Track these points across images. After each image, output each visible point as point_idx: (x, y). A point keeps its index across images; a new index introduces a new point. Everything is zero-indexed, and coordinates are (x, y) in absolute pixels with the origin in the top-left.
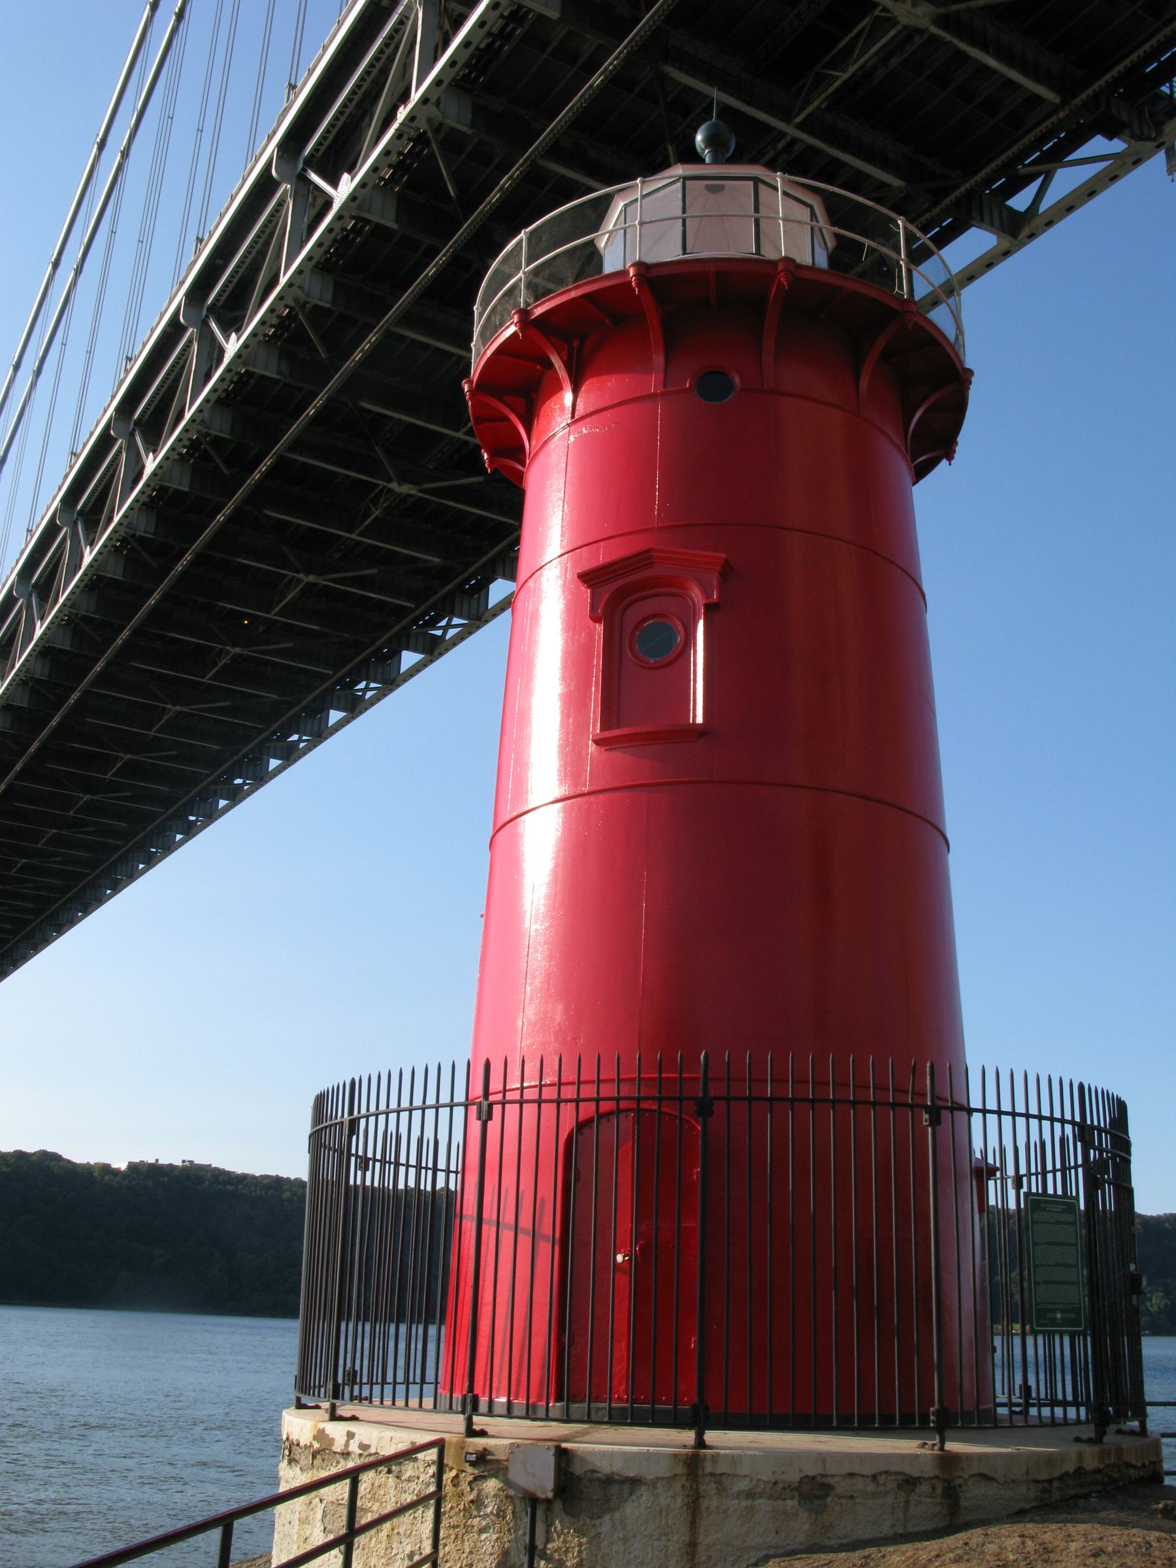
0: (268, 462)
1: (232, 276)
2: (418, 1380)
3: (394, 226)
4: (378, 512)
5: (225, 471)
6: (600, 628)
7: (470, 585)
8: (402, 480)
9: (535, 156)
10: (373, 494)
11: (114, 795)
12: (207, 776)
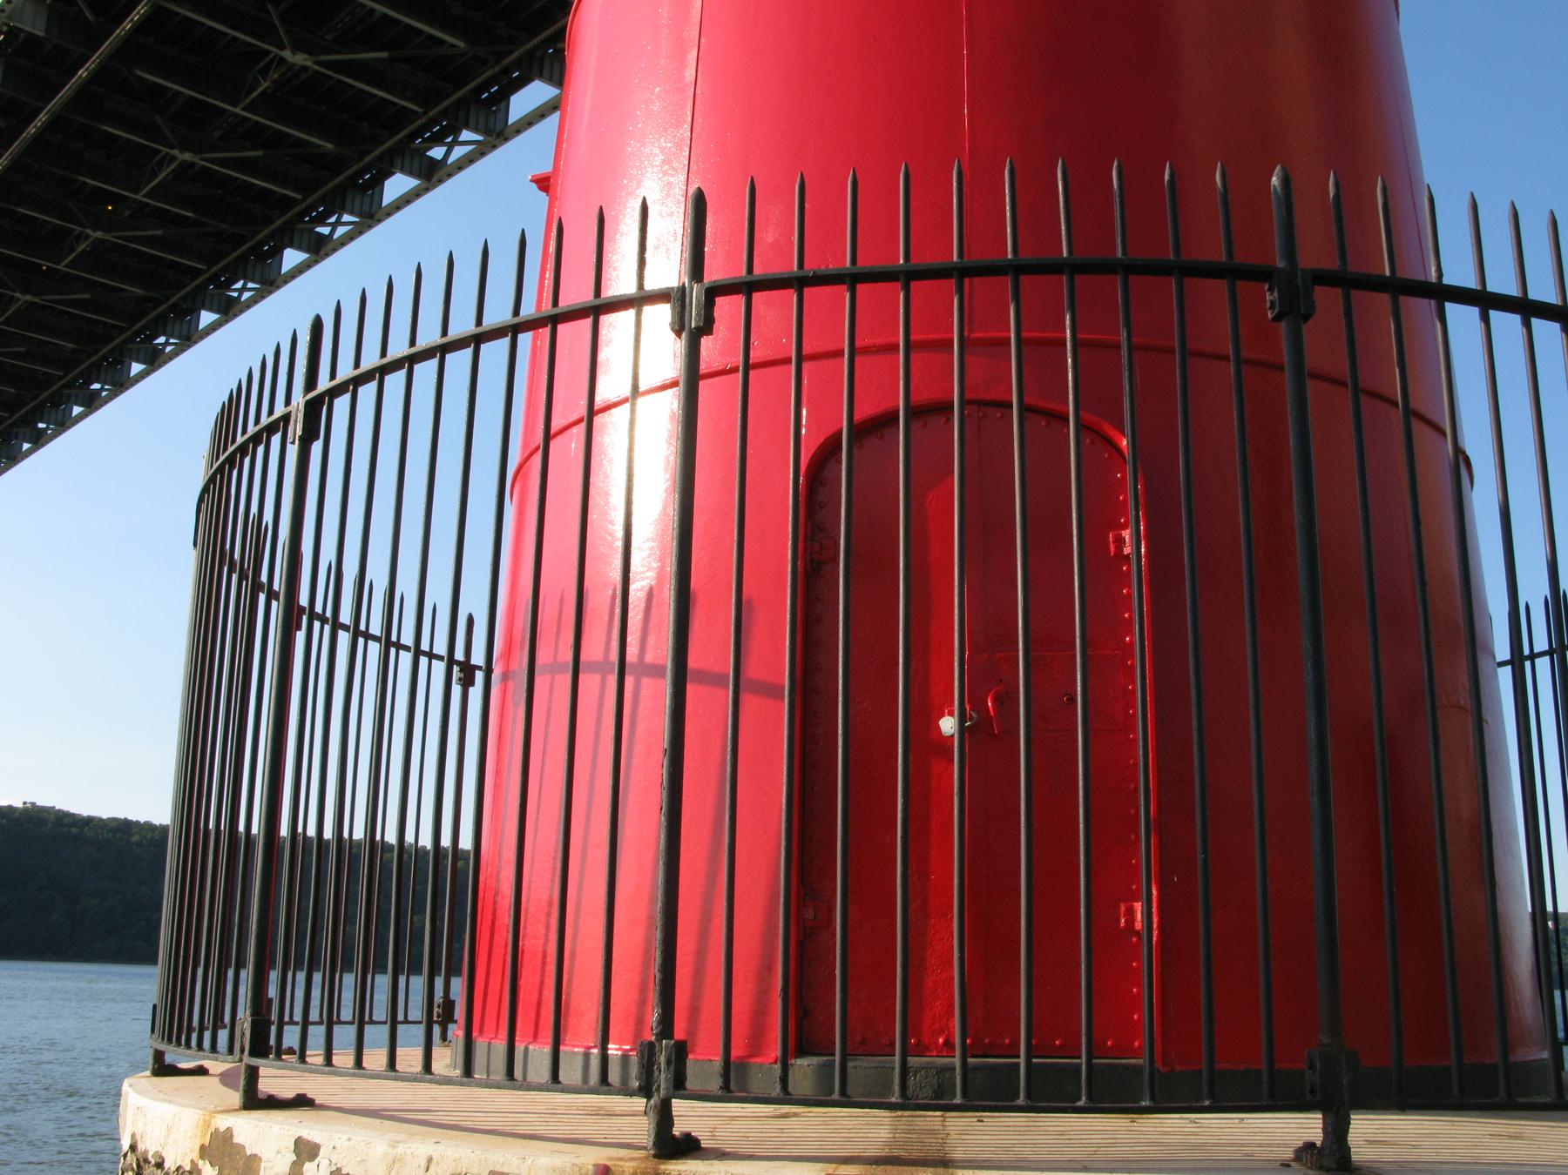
2: (298, 1017)
4: (268, 83)
8: (297, 48)
10: (261, 65)
12: (61, 378)
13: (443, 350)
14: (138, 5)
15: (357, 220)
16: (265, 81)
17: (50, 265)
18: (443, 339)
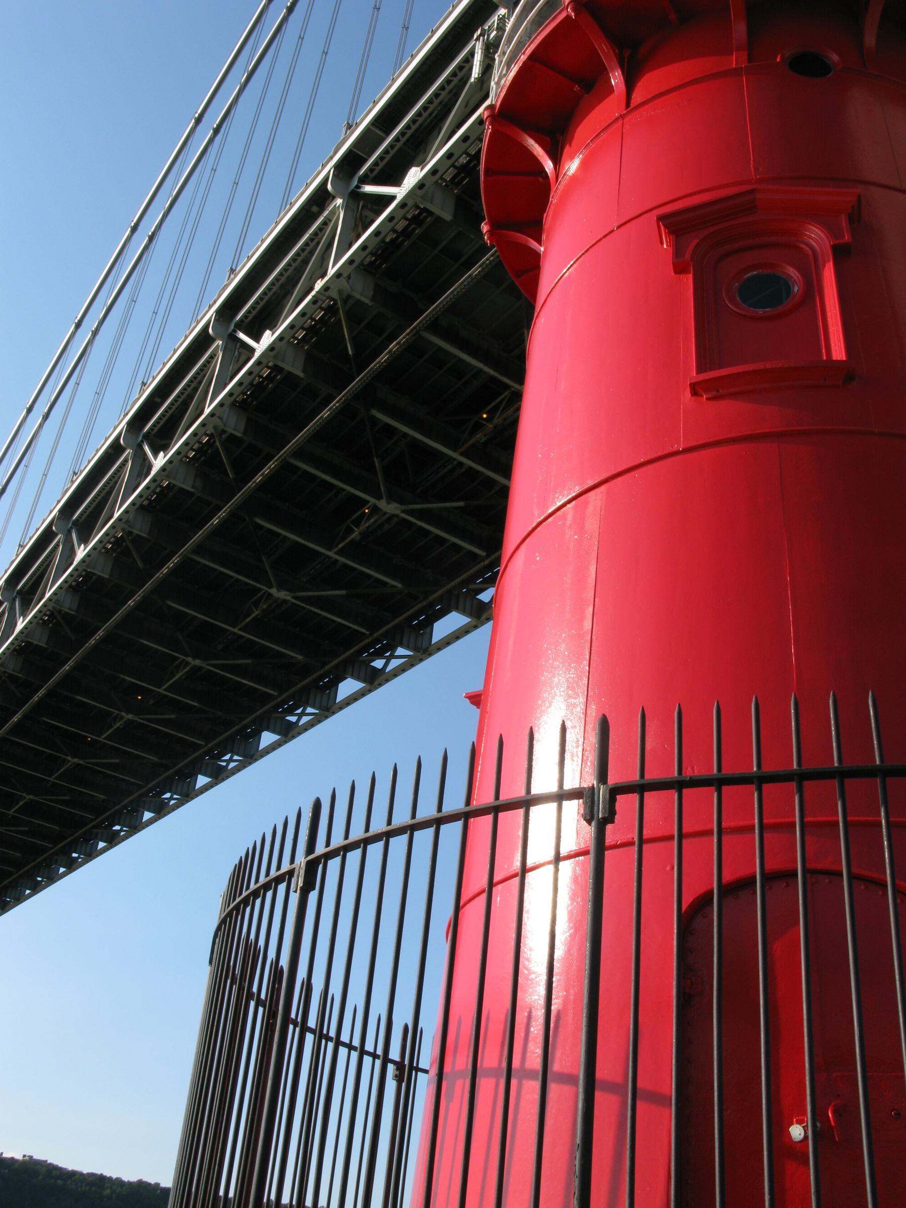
0: (175, 559)
1: (166, 411)
3: (301, 375)
5: (140, 565)
6: (689, 280)
7: (324, 683)
8: (280, 587)
9: (420, 327)
11: (15, 829)
12: (92, 820)
13: (412, 829)
14: (174, 556)
15: (317, 712)
16: (257, 610)
17: (94, 737)
18: (413, 821)
